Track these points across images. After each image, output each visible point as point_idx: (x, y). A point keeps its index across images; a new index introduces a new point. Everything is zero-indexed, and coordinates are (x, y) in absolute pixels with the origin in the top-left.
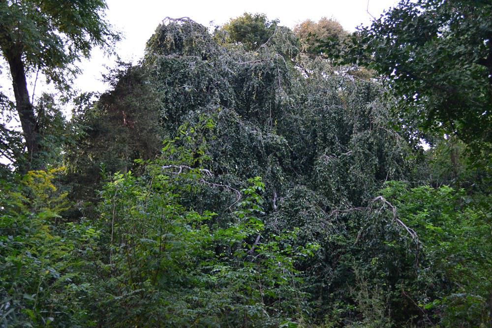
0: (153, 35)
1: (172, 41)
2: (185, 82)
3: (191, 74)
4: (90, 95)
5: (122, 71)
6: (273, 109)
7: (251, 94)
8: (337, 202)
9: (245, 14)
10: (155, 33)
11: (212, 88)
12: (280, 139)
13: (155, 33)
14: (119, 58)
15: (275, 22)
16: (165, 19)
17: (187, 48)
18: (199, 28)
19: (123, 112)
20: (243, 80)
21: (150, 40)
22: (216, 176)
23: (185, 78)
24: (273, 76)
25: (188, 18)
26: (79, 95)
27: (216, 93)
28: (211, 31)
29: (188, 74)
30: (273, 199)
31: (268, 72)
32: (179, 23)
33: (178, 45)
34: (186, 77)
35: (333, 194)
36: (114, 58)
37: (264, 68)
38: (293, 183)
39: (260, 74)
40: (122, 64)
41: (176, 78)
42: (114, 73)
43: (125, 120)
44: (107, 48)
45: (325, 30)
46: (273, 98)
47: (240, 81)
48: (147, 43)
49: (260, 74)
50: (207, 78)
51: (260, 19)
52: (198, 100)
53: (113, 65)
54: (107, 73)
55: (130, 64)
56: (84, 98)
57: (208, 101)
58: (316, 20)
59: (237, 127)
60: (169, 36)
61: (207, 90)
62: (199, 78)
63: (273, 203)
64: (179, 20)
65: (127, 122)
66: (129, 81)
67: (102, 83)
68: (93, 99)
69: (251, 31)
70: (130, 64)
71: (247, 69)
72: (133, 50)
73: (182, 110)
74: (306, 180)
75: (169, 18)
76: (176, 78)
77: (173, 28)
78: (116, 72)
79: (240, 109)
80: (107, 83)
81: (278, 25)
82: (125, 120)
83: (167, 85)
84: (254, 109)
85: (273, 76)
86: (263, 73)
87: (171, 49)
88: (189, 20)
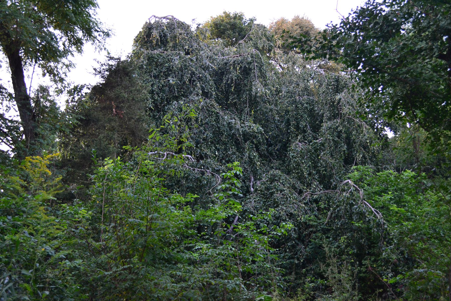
0: (140, 32)
1: (157, 37)
2: (169, 75)
3: (175, 68)
4: (82, 87)
5: (112, 65)
6: (250, 100)
7: (230, 86)
8: (309, 185)
9: (225, 13)
10: (142, 30)
11: (194, 81)
12: (256, 128)
13: (142, 30)
14: (109, 53)
15: (252, 20)
16: (151, 17)
17: (171, 44)
18: (182, 25)
19: (113, 102)
20: (222, 74)
21: (137, 37)
22: (198, 161)
23: (169, 71)
24: (250, 70)
25: (172, 16)
26: (72, 87)
27: (198, 85)
28: (193, 28)
29: (173, 68)
30: (250, 182)
31: (245, 66)
32: (164, 21)
33: (163, 41)
34: (171, 70)
35: (305, 178)
36: (104, 53)
37: (242, 62)
38: (269, 168)
39: (238, 68)
40: (111, 58)
41: (161, 72)
42: (104, 67)
43: (114, 110)
44: (98, 44)
45: (298, 27)
46: (251, 90)
47: (220, 74)
48: (135, 39)
49: (238, 68)
50: (190, 72)
51: (239, 17)
52: (181, 92)
53: (103, 59)
54: (98, 66)
55: (119, 59)
56: (77, 89)
57: (191, 93)
58: (290, 18)
59: (217, 116)
60: (155, 33)
61: (190, 83)
62: (182, 71)
63: (250, 186)
64: (164, 18)
65: (116, 112)
66: (118, 74)
67: (94, 76)
68: (85, 90)
69: (230, 29)
70: (119, 59)
71: (226, 64)
72: (122, 47)
73: (167, 101)
74: (280, 165)
75: (155, 16)
76: (161, 72)
77: (158, 25)
78: (106, 66)
79: (220, 100)
80: (98, 76)
81: (255, 22)
82: (114, 110)
83: (153, 78)
84: (232, 100)
85: (250, 70)
86: (241, 67)
87: (157, 45)
88: (173, 18)
